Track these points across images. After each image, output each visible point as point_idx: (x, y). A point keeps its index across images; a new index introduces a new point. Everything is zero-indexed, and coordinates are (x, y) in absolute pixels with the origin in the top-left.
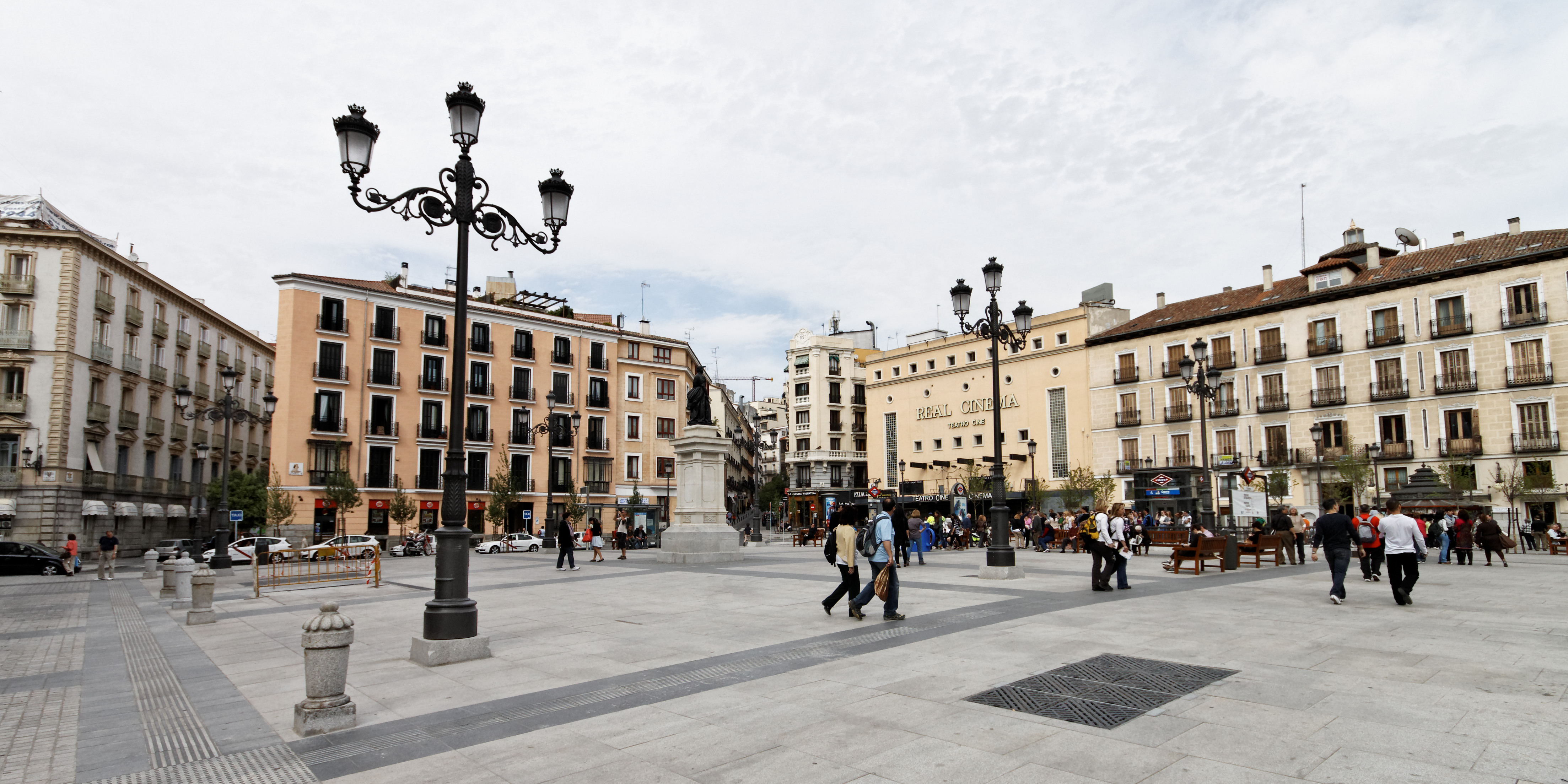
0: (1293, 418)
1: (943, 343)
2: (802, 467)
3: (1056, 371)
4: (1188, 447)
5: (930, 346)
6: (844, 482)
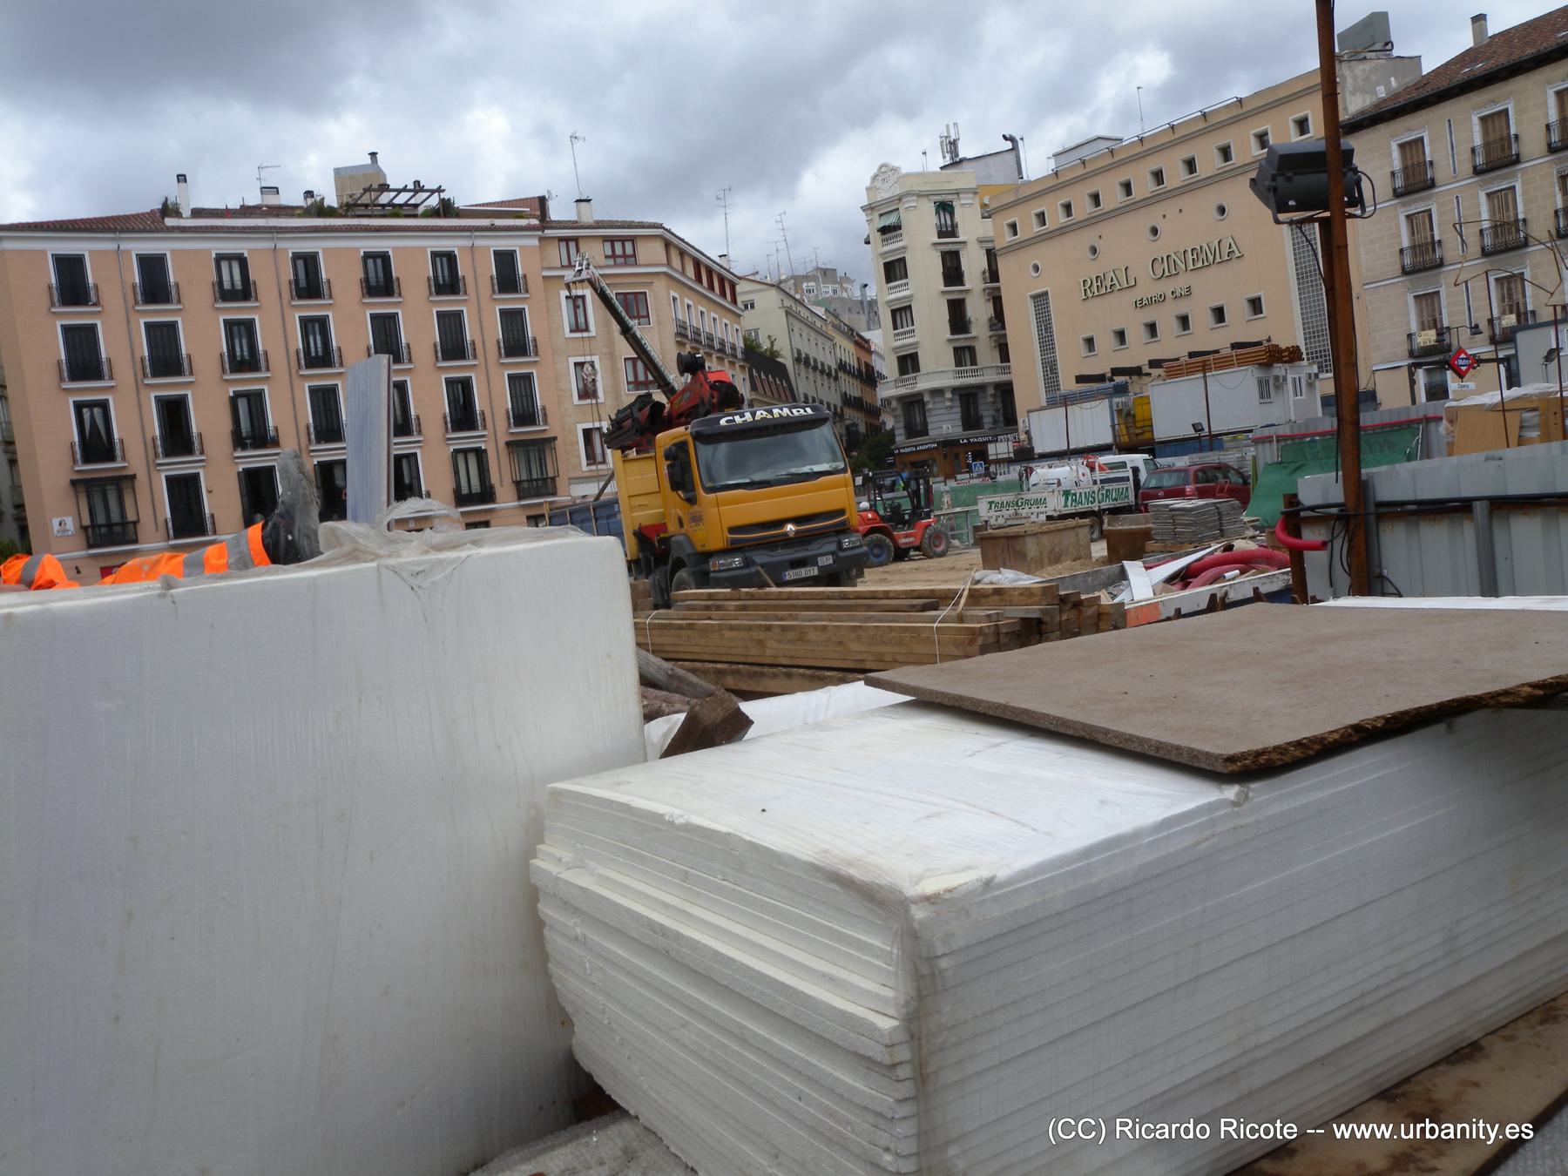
1: (1111, 160)
3: (1222, 210)
4: (1524, 296)
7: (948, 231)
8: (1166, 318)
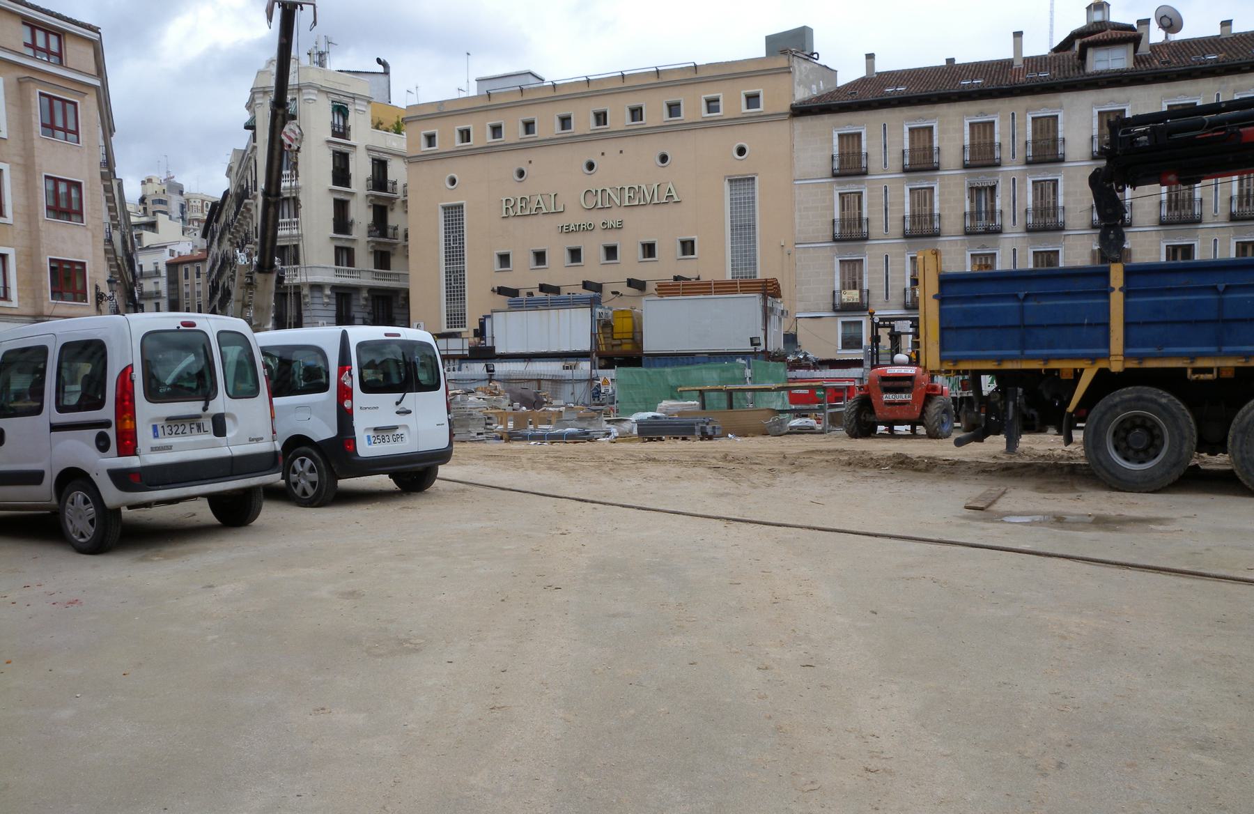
0: (1069, 241)
3: (664, 158)
5: (527, 97)
7: (341, 132)
8: (593, 247)
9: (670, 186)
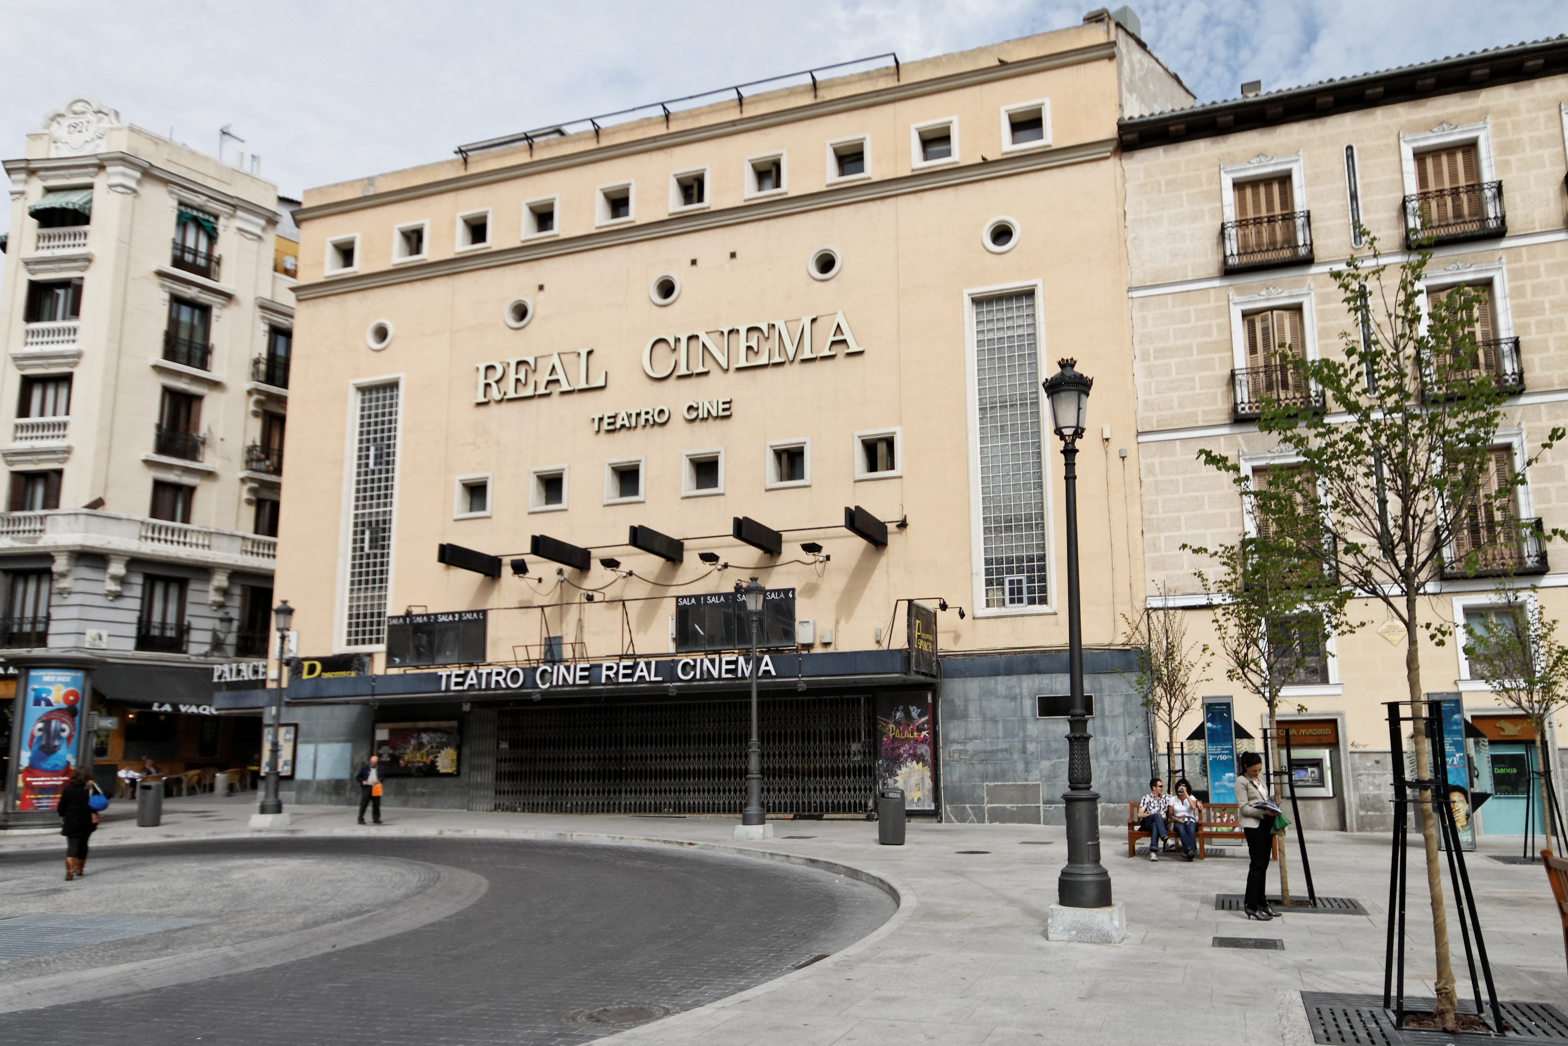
2: (24, 575)
6: (194, 636)
9: (840, 319)
